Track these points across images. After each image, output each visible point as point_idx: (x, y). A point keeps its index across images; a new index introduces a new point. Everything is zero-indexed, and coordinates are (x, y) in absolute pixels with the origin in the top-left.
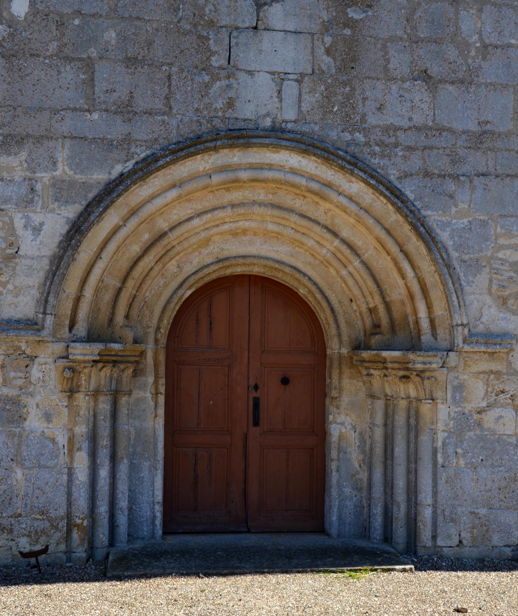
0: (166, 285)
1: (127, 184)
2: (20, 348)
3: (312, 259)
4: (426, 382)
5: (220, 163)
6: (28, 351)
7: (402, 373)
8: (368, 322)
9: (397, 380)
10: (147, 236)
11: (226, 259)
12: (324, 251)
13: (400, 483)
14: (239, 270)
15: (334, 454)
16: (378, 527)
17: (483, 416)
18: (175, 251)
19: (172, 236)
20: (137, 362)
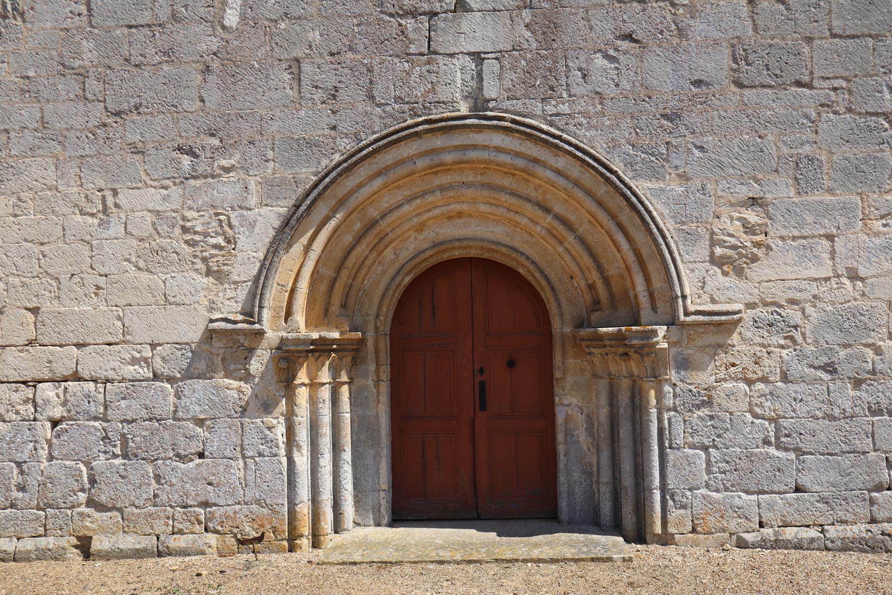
0: (384, 272)
2: (238, 341)
3: (529, 238)
4: (646, 359)
5: (423, 148)
6: (246, 344)
7: (621, 350)
8: (588, 298)
9: (618, 358)
10: (358, 226)
11: (443, 243)
12: (539, 229)
13: (627, 466)
14: (457, 254)
16: (608, 513)
18: (388, 238)
19: (383, 224)
20: (357, 350)
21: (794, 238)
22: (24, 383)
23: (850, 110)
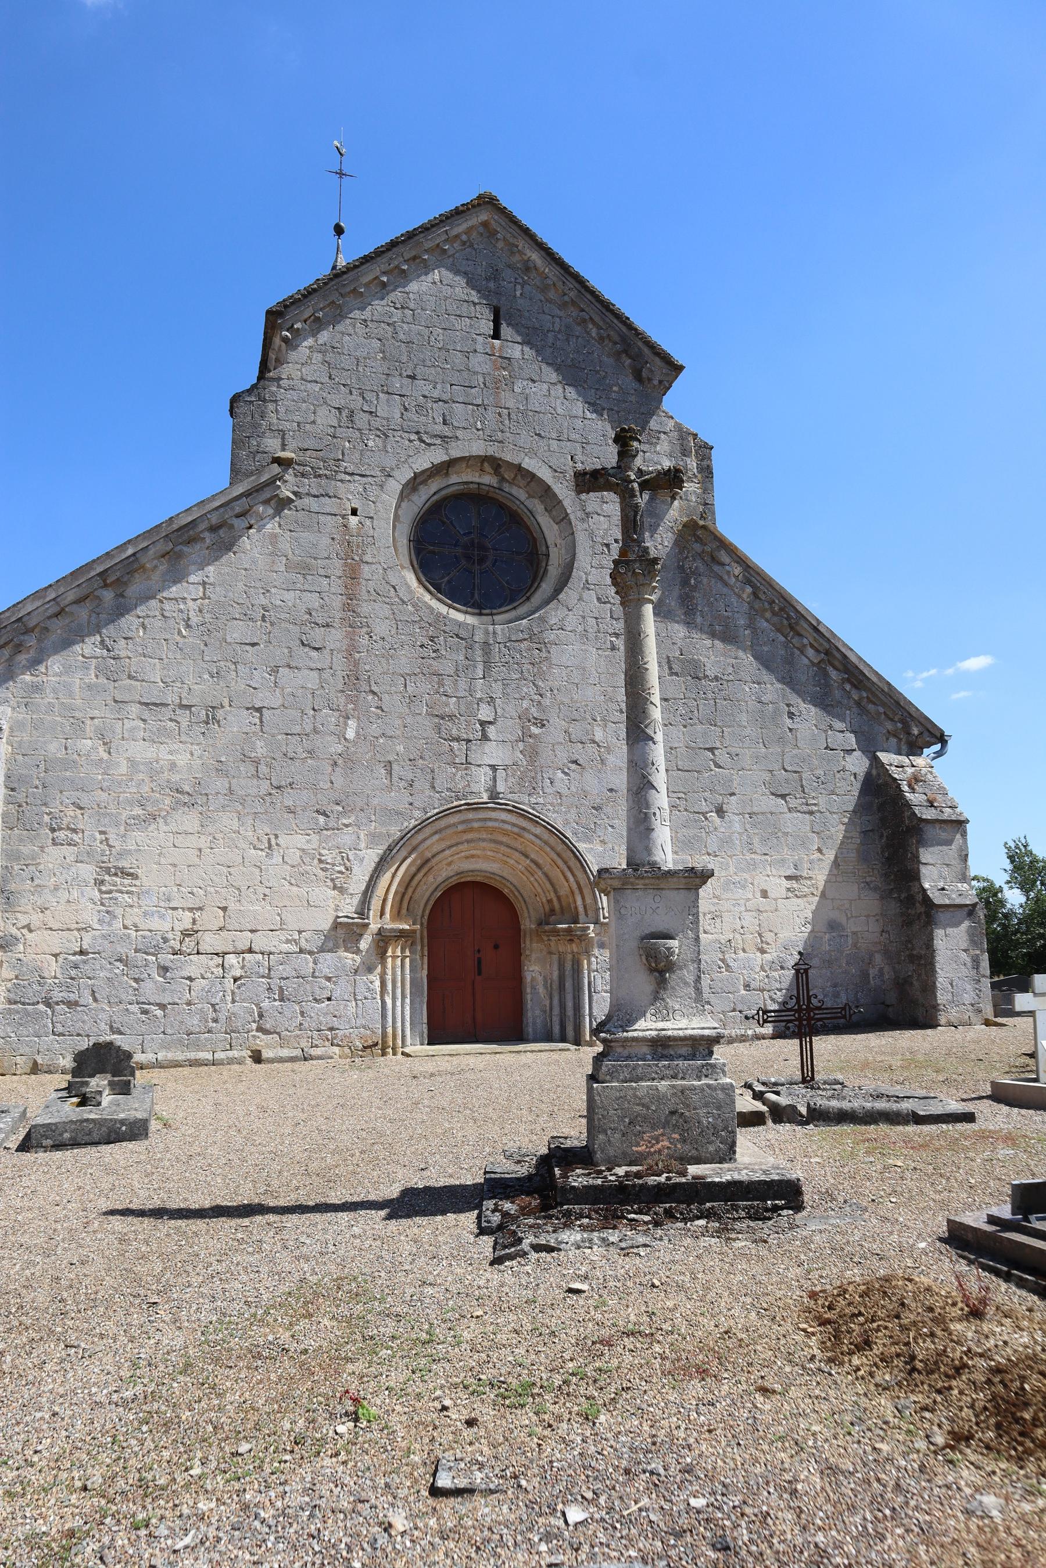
23: (686, 810)
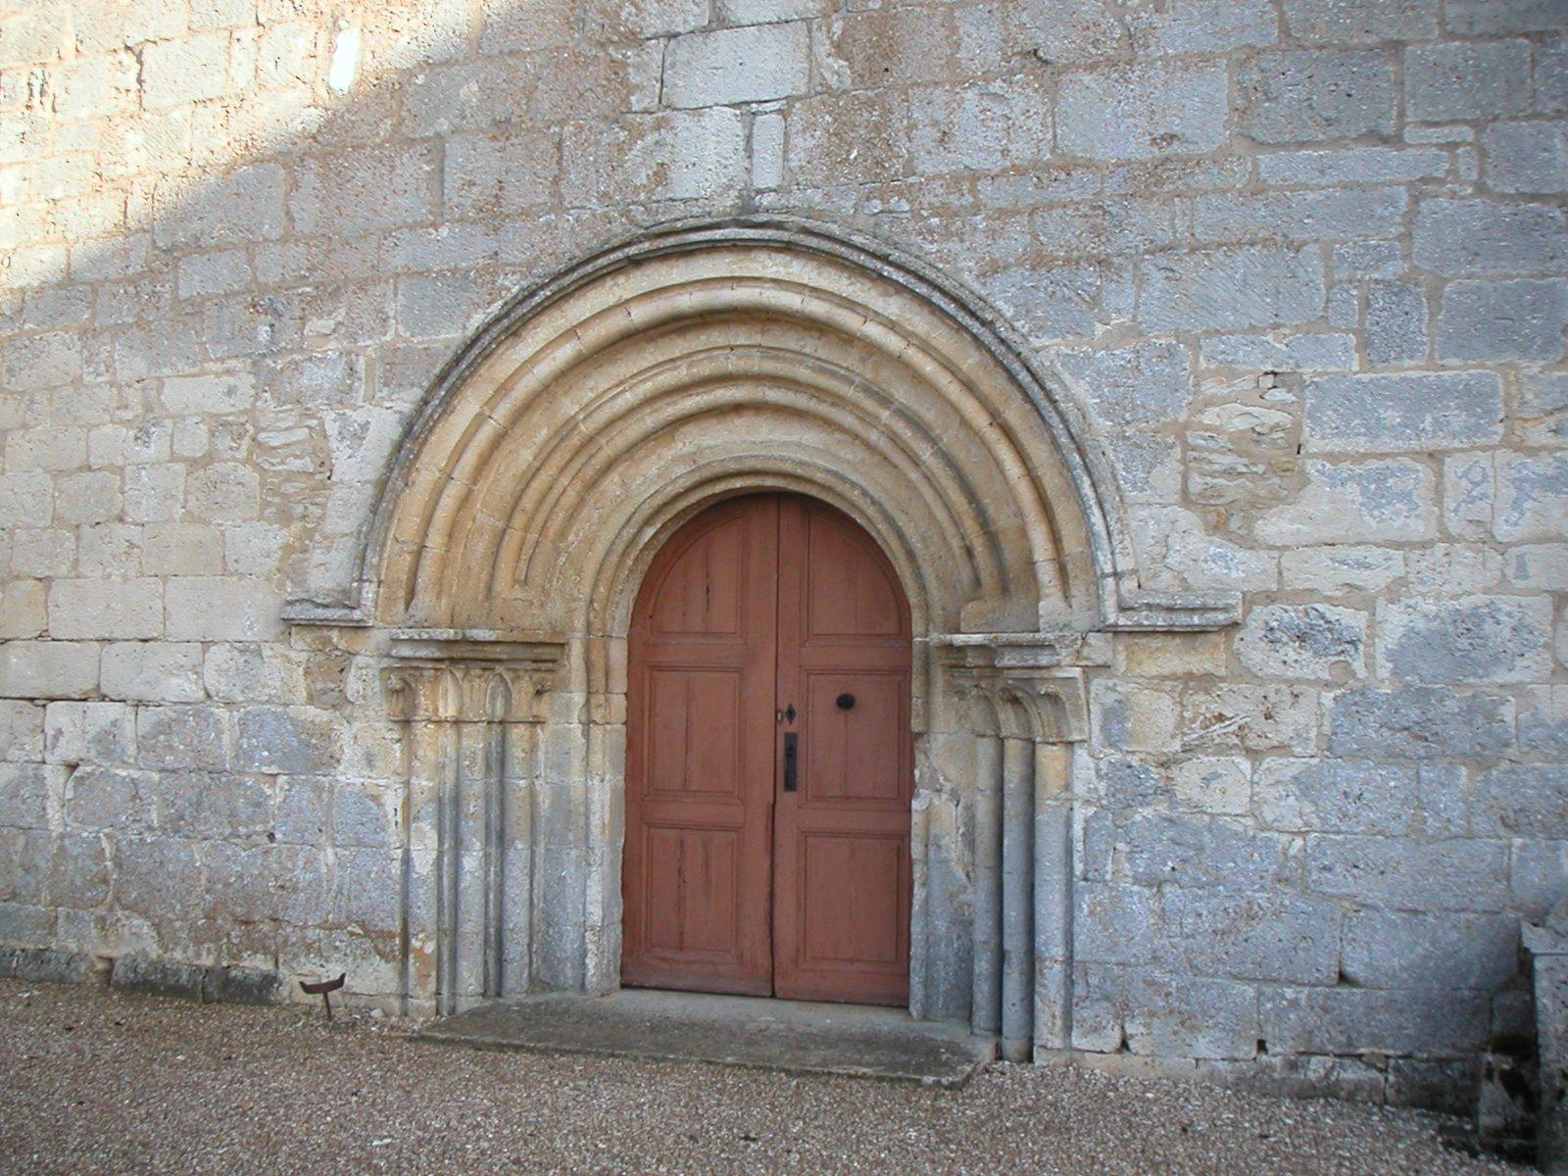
1: (1306, 786)
2: (330, 640)
6: (342, 645)
13: (1013, 913)
15: (916, 850)
17: (1174, 772)
21: (1362, 458)
22: (32, 699)
